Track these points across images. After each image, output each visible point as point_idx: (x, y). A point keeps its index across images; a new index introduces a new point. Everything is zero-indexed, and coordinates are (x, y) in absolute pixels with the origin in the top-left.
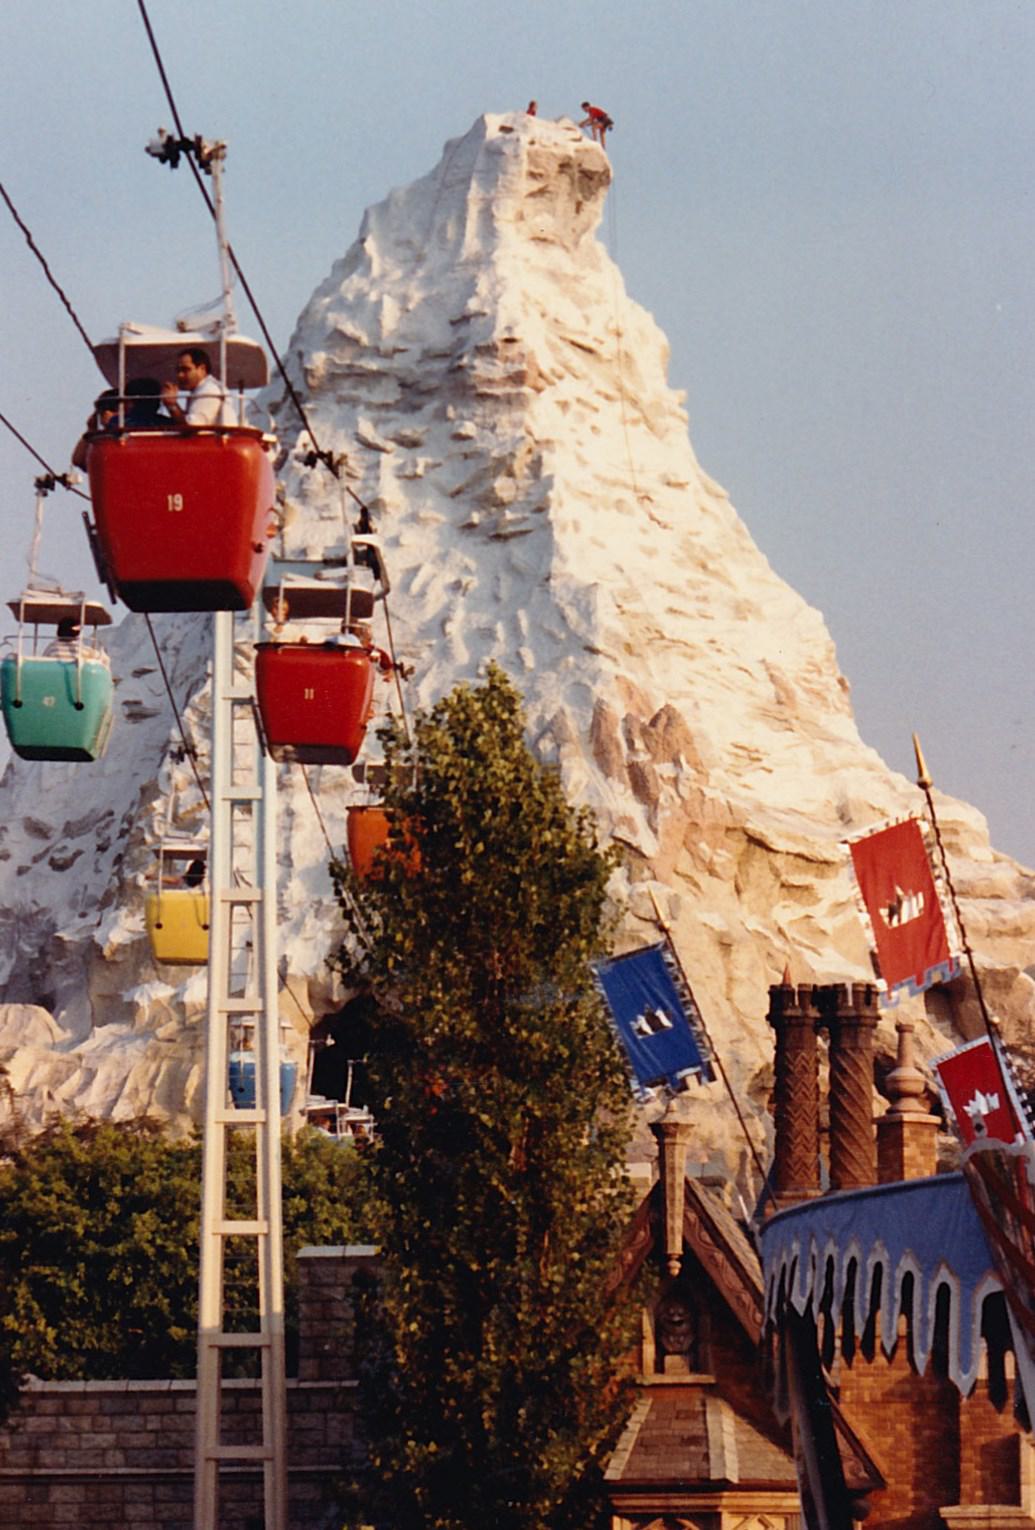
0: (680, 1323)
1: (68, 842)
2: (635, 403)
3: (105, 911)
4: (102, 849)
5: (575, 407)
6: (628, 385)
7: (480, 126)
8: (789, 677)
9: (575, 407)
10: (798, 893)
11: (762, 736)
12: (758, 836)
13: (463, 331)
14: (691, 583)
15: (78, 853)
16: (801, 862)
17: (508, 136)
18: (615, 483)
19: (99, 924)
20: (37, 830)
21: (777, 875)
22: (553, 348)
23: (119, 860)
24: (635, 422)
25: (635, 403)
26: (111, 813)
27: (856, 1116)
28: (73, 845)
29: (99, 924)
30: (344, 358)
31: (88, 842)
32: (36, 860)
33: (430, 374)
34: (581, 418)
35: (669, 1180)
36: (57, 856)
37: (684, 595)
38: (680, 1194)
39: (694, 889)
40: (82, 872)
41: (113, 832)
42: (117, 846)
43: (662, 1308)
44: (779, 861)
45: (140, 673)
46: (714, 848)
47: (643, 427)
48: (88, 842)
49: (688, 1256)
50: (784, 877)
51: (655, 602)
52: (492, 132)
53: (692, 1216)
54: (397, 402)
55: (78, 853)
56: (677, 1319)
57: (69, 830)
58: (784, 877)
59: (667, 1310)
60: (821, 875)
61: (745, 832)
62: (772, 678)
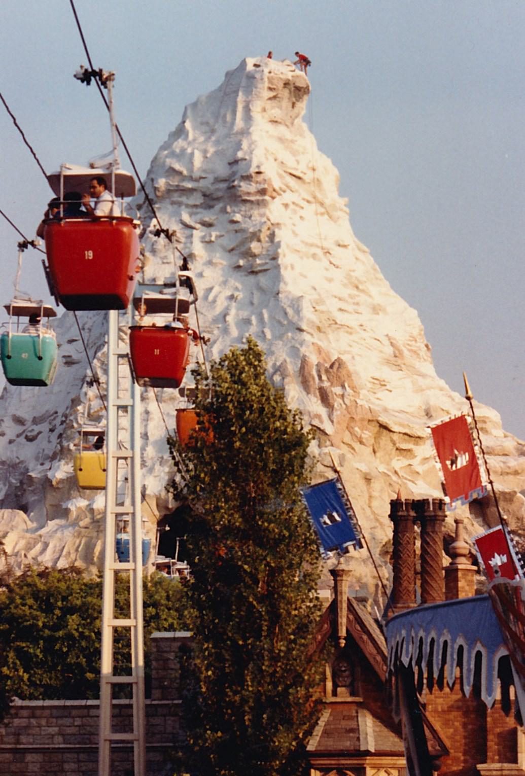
0: (345, 671)
1: (34, 427)
2: (322, 204)
3: (53, 462)
4: (52, 430)
5: (292, 206)
6: (318, 195)
7: (243, 64)
8: (400, 343)
9: (292, 206)
10: (405, 453)
11: (387, 373)
12: (384, 424)
13: (235, 168)
14: (350, 296)
15: (40, 433)
16: (406, 437)
17: (258, 69)
18: (312, 245)
19: (50, 469)
20: (19, 421)
21: (394, 444)
22: (281, 176)
23: (60, 436)
24: (322, 214)
25: (322, 204)
26: (56, 413)
27: (434, 566)
28: (37, 429)
29: (50, 469)
30: (175, 182)
31: (44, 427)
32: (18, 436)
33: (218, 190)
34: (295, 212)
35: (339, 598)
36: (29, 434)
37: (347, 302)
38: (345, 605)
39: (352, 451)
40: (42, 442)
41: (57, 422)
42: (59, 429)
43: (336, 664)
44: (395, 437)
45: (71, 341)
46: (362, 430)
47: (326, 217)
48: (44, 427)
49: (349, 637)
50: (398, 445)
51: (332, 306)
52: (250, 67)
53: (351, 617)
54: (202, 204)
55: (40, 433)
56: (343, 669)
57: (35, 421)
58: (398, 445)
59: (338, 665)
60: (416, 444)
61: (378, 422)
62: (392, 344)
